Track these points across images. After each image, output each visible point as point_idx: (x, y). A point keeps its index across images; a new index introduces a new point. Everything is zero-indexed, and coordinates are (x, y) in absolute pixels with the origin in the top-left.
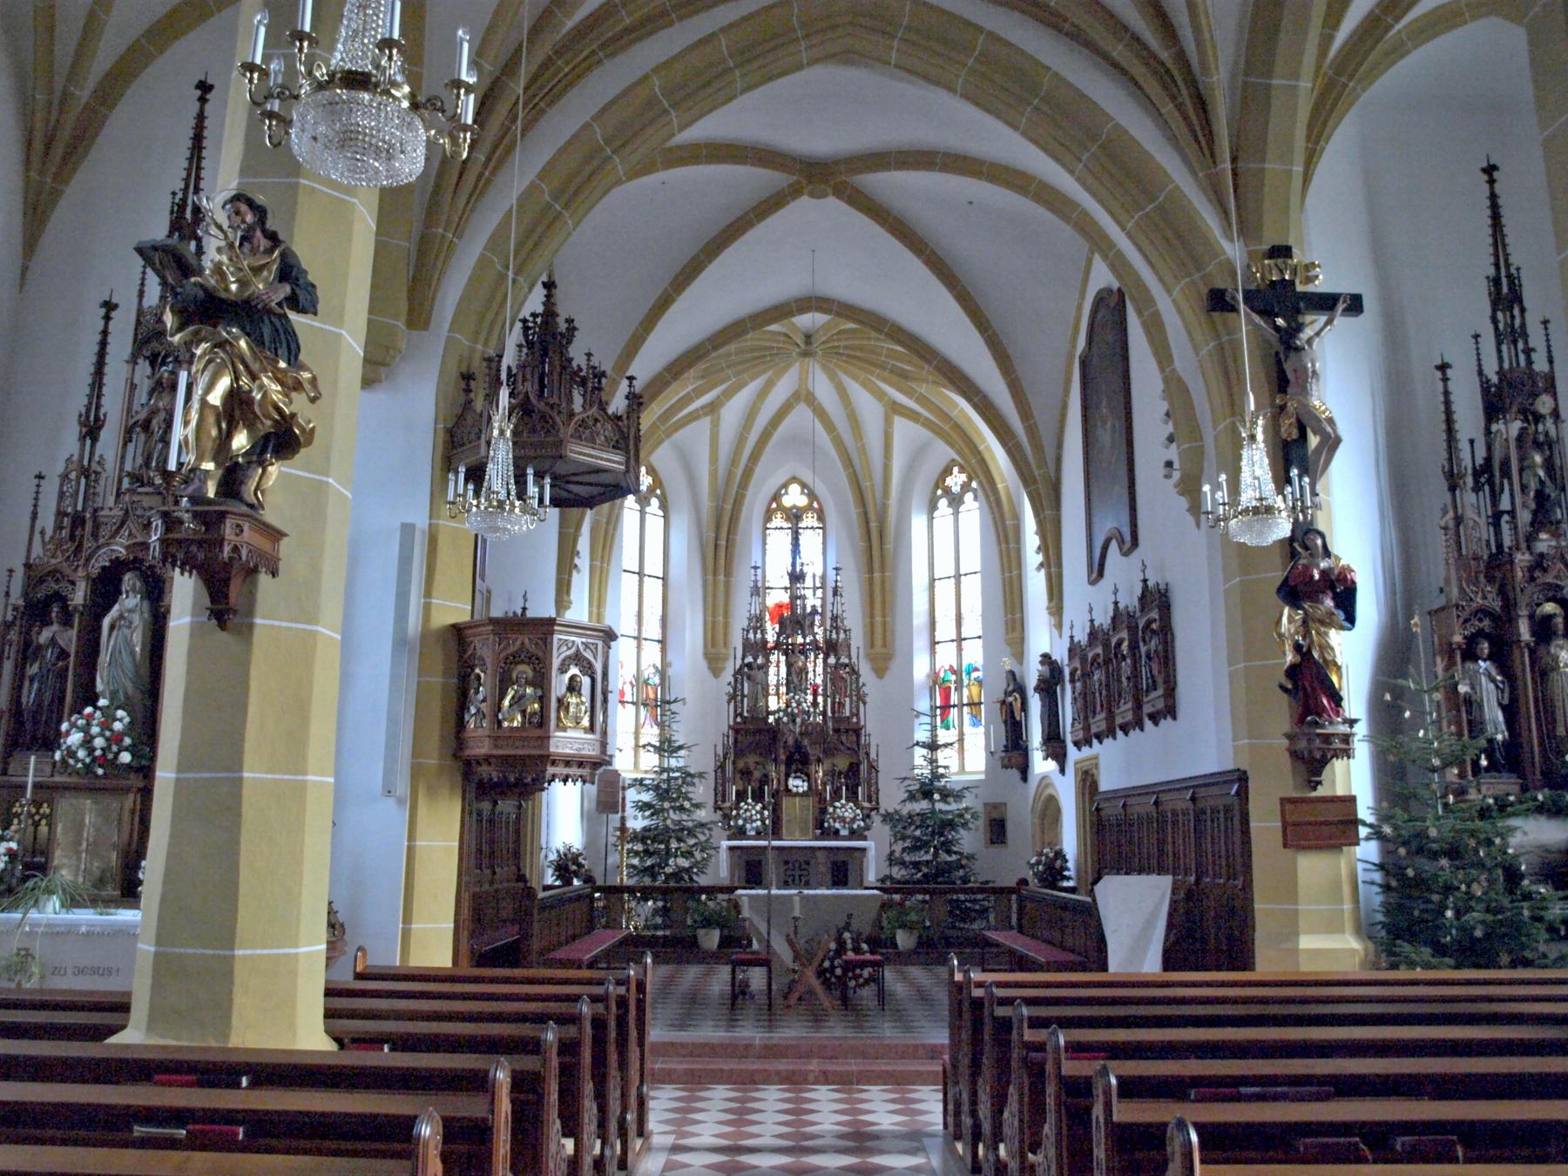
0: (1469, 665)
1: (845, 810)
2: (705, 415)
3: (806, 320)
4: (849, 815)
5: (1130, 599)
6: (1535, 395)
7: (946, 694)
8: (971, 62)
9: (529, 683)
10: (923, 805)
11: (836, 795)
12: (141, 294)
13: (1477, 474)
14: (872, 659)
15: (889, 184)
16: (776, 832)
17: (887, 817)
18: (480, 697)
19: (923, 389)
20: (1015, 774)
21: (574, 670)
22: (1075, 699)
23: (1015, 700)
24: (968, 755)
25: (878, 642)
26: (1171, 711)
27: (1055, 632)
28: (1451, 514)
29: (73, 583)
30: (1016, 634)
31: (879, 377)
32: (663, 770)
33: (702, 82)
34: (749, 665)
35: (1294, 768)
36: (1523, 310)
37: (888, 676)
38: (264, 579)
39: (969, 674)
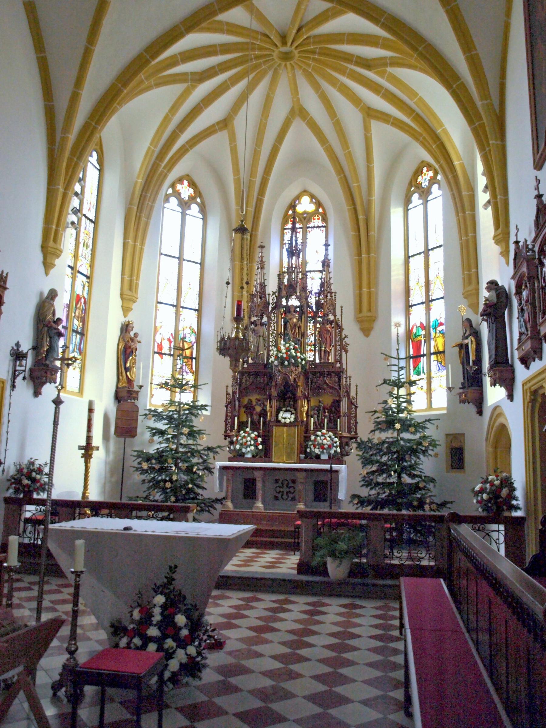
1: (325, 438)
2: (221, 129)
4: (326, 442)
7: (417, 346)
10: (389, 435)
11: (319, 426)
14: (360, 321)
16: (266, 453)
17: (361, 445)
20: (472, 408)
23: (470, 341)
24: (431, 395)
27: (503, 260)
30: (472, 287)
32: (172, 402)
37: (373, 333)
39: (435, 328)
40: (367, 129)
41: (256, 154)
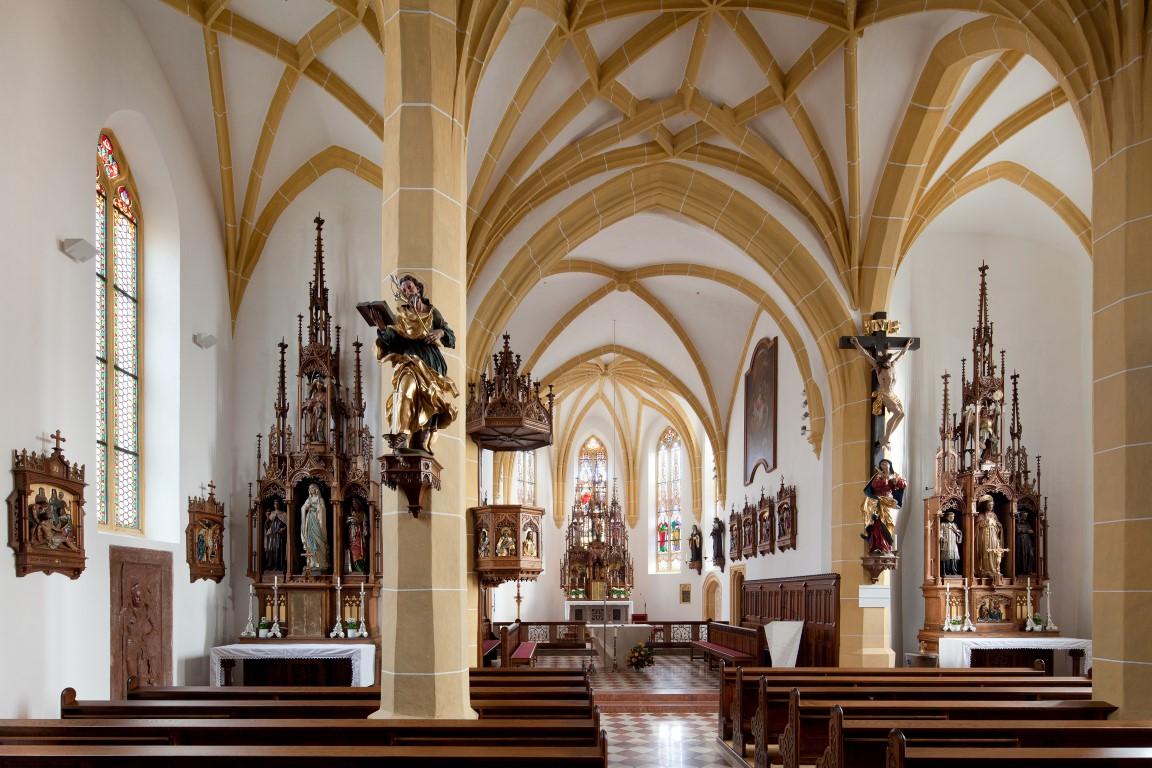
0: (943, 524)
3: (609, 357)
5: (772, 492)
6: (993, 391)
8: (723, 210)
9: (509, 536)
12: (300, 339)
13: (955, 431)
15: (658, 284)
18: (486, 542)
19: (659, 392)
20: (695, 571)
21: (529, 530)
22: (732, 539)
24: (586, 547)
25: (632, 512)
26: (794, 546)
28: (942, 452)
29: (284, 490)
31: (639, 386)
33: (582, 223)
34: (575, 523)
35: (865, 574)
36: (991, 346)
38: (434, 491)
40: (640, 408)
41: (570, 417)
